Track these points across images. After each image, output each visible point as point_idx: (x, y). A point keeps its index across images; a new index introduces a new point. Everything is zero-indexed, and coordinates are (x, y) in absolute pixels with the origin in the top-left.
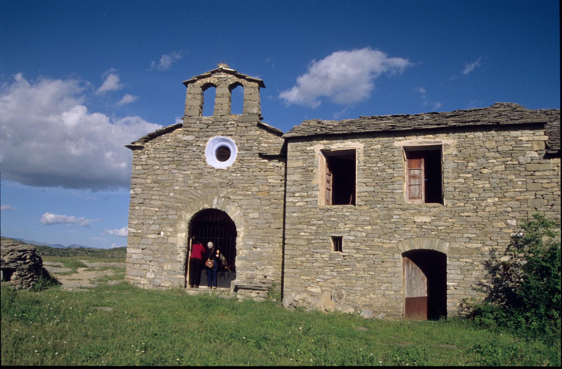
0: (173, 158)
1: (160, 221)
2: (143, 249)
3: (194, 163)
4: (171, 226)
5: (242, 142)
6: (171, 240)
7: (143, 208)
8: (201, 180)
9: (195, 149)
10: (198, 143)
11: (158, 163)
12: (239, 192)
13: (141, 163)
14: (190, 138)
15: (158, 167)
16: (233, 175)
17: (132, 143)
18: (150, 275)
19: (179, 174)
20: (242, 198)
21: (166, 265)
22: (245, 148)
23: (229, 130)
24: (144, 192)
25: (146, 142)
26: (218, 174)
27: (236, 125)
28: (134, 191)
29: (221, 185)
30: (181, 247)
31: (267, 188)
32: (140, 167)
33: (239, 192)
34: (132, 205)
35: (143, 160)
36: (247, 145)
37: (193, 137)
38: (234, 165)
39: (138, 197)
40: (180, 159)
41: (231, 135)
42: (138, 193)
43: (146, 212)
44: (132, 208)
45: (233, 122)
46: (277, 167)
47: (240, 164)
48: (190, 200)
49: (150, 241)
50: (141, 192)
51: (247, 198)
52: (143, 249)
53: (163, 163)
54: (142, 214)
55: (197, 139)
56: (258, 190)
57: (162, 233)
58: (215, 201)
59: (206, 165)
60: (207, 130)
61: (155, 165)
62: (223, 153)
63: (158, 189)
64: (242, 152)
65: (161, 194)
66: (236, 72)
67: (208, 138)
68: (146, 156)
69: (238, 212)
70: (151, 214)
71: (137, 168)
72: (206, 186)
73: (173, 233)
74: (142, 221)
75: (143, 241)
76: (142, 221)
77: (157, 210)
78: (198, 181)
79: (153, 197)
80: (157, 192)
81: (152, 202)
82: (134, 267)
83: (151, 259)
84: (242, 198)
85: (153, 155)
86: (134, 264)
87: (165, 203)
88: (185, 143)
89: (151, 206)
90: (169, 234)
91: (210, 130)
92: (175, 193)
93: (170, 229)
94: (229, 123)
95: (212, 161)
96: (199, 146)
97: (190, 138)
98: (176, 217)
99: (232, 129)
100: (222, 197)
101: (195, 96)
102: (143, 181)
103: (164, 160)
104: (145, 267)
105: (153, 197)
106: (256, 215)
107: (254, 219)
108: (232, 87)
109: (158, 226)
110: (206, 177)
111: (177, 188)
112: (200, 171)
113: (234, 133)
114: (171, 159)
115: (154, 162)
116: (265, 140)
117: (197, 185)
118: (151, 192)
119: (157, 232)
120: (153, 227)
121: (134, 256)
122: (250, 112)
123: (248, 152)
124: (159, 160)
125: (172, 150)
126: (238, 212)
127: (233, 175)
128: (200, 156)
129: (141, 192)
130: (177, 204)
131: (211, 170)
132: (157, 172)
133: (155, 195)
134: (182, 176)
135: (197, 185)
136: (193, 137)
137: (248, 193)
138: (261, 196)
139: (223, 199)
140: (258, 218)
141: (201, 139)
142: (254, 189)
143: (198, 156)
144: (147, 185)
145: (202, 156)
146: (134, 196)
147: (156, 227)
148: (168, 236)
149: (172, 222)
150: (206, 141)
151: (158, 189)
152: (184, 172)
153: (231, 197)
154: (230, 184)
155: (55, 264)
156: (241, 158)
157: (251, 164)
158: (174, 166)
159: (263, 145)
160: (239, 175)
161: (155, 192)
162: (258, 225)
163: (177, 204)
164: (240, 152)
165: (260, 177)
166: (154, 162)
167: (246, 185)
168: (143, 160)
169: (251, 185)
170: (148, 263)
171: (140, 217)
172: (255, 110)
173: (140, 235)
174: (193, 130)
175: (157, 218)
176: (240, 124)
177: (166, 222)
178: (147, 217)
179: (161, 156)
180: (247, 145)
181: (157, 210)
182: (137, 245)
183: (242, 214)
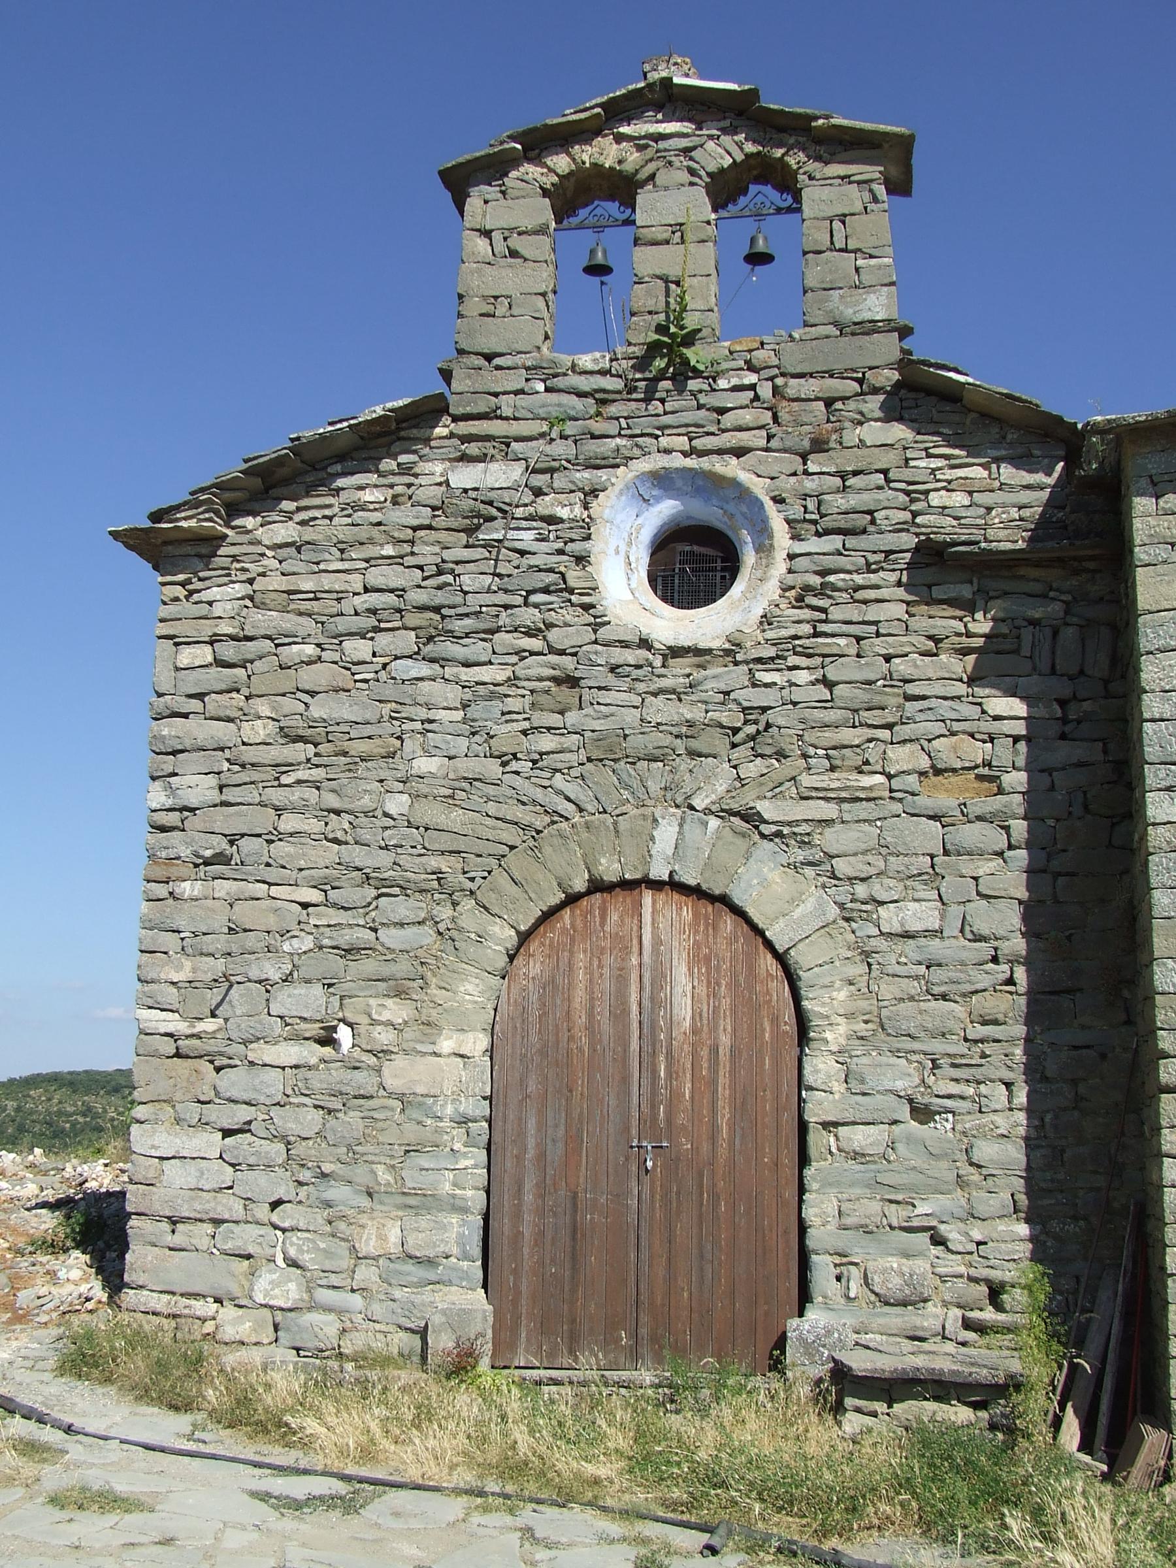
0: (400, 592)
1: (335, 963)
2: (227, 1133)
3: (529, 616)
4: (400, 993)
5: (810, 484)
6: (399, 1074)
7: (223, 888)
8: (572, 718)
9: (529, 535)
10: (545, 505)
11: (307, 625)
12: (806, 780)
13: (207, 629)
14: (499, 475)
15: (310, 650)
16: (767, 677)
17: (156, 517)
18: (276, 1287)
19: (438, 686)
20: (829, 810)
21: (371, 1230)
22: (827, 523)
23: (728, 420)
24: (230, 795)
25: (233, 510)
26: (677, 674)
27: (765, 390)
28: (171, 791)
29: (689, 740)
30: (463, 1121)
31: (978, 751)
32: (205, 654)
33: (806, 780)
34: (160, 873)
35: (217, 610)
36: (840, 502)
37: (515, 473)
38: (766, 620)
39: (193, 822)
40: (440, 598)
41: (739, 452)
42: (194, 802)
43: (244, 913)
44: (161, 890)
45: (751, 378)
46: (1033, 623)
47: (806, 614)
48: (510, 835)
49: (273, 1084)
50: (214, 796)
51: (863, 810)
52: (227, 1133)
53: (342, 624)
54: (219, 922)
55: (540, 480)
56: (924, 763)
57: (344, 1034)
58: (666, 835)
59: (596, 627)
60: (598, 426)
61: (292, 638)
62: (694, 562)
63: (318, 774)
64: (813, 545)
65: (333, 801)
66: (753, 94)
67: (603, 475)
68: (240, 589)
69: (809, 905)
70: (272, 922)
71: (186, 656)
72: (608, 751)
73: (408, 1034)
74: (220, 965)
75: (234, 1082)
76: (220, 965)
77: (314, 896)
78: (555, 720)
79: (289, 823)
80: (311, 794)
81: (281, 849)
82: (177, 1240)
83: (281, 1193)
84: (829, 810)
85: (276, 582)
86: (173, 1221)
87: (357, 855)
88: (466, 504)
89: (273, 874)
90: (384, 1037)
91: (612, 428)
92: (416, 796)
93: (395, 1010)
94: (722, 383)
95: (620, 579)
96: (551, 520)
97: (499, 475)
98: (426, 935)
99: (747, 417)
100: (708, 811)
101: (516, 242)
102: (222, 732)
103: (347, 606)
104: (245, 1237)
105: (289, 823)
106: (919, 914)
107: (907, 935)
108: (725, 189)
109: (317, 990)
110: (604, 697)
111: (424, 765)
112: (568, 662)
113: (757, 439)
114: (391, 599)
115: (289, 622)
116: (950, 474)
117: (547, 742)
118: (276, 796)
119: (314, 1029)
120: (288, 1001)
121: (177, 1176)
122: (849, 313)
123: (851, 542)
124: (315, 606)
125: (389, 550)
126: (809, 905)
127: (767, 677)
128: (571, 590)
129: (214, 796)
130: (434, 862)
131: (631, 656)
132: (308, 677)
133: (300, 809)
134: (454, 694)
135: (547, 742)
136: (515, 473)
137: (867, 781)
138: (946, 801)
139: (714, 823)
140: (938, 933)
141: (560, 481)
142: (903, 757)
143: (550, 578)
144: (249, 755)
145: (574, 577)
146: (173, 818)
147: (306, 1000)
148: (382, 1053)
149: (403, 967)
150: (593, 492)
151: (318, 774)
152: (466, 674)
153: (766, 809)
154: (753, 732)
155: (635, 949)
156: (816, 580)
157: (873, 613)
158: (407, 641)
159: (935, 499)
160: (803, 677)
161: (297, 794)
162: (937, 975)
163: (434, 862)
164: (799, 547)
165: (938, 689)
166: (289, 622)
167: (848, 735)
168: (217, 610)
169: (885, 734)
170: (262, 1212)
171: (209, 943)
172: (877, 305)
173: (211, 1046)
174: (515, 428)
175: (308, 943)
176: (794, 387)
177: (369, 966)
178: (250, 940)
179: (327, 582)
180: (840, 502)
181: (314, 896)
182: (193, 1111)
183: (833, 912)
